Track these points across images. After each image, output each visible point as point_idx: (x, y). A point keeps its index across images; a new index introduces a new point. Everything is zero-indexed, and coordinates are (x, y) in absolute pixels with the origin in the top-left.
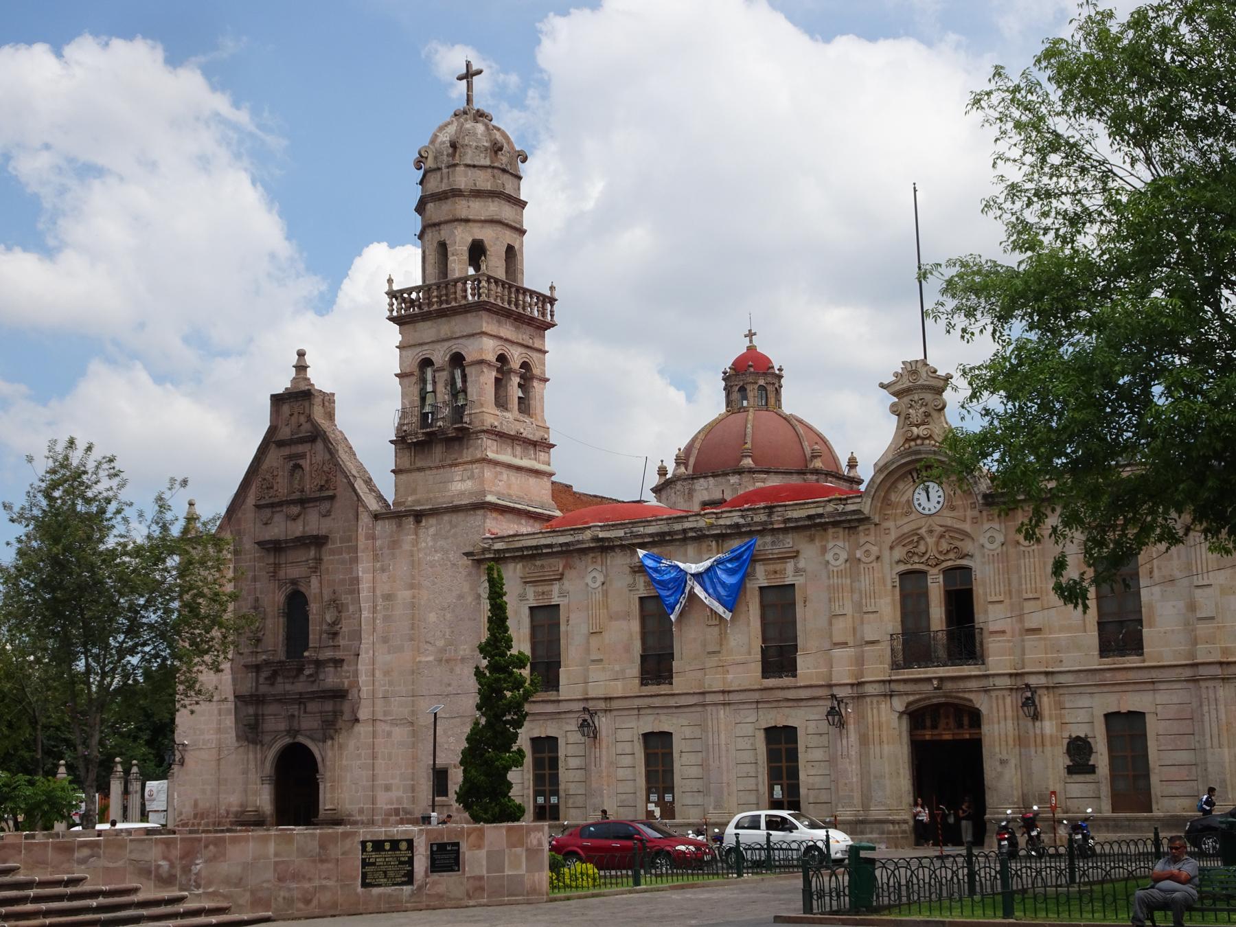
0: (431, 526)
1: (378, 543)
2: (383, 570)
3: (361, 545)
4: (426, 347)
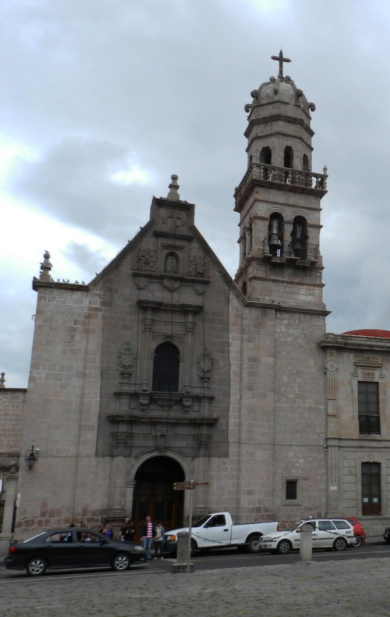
0: (286, 318)
1: (246, 322)
2: (250, 341)
3: (231, 321)
4: (278, 206)
